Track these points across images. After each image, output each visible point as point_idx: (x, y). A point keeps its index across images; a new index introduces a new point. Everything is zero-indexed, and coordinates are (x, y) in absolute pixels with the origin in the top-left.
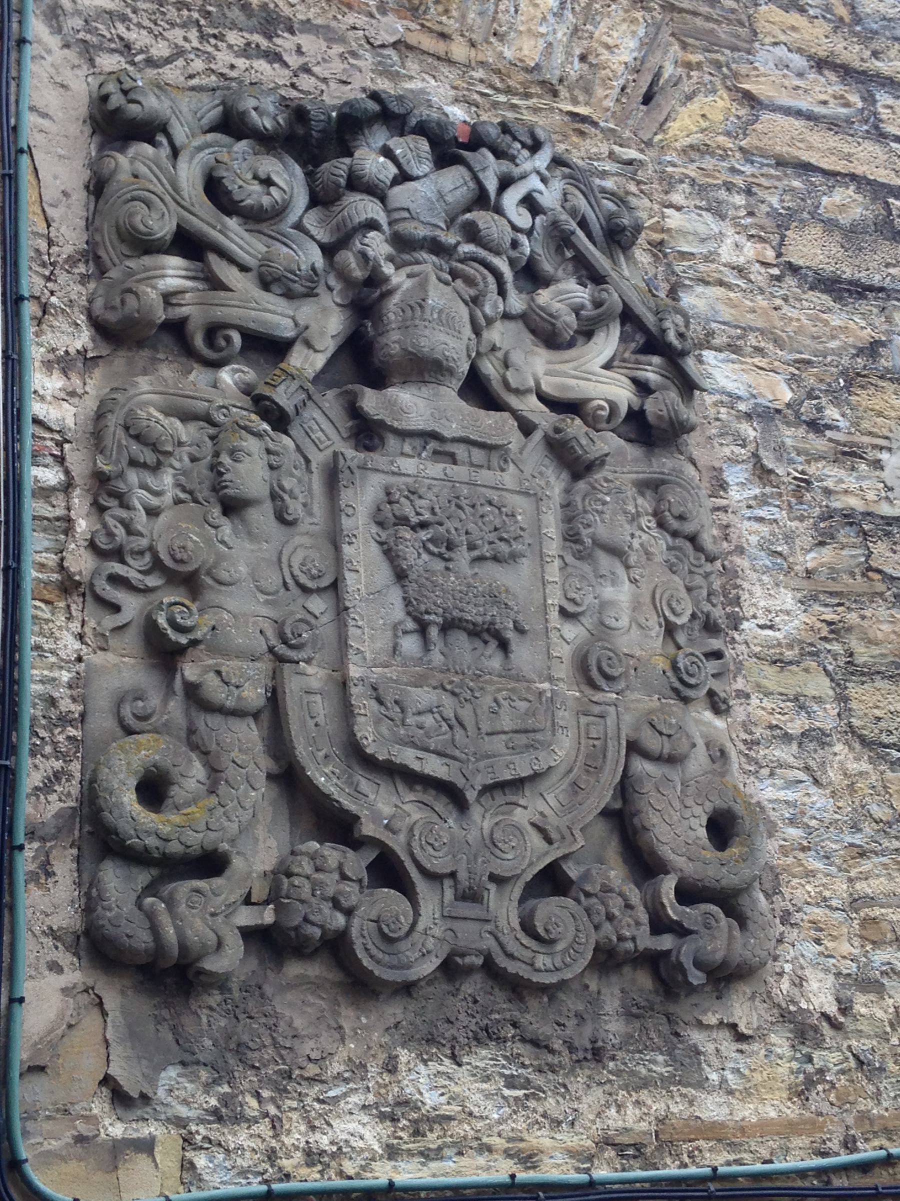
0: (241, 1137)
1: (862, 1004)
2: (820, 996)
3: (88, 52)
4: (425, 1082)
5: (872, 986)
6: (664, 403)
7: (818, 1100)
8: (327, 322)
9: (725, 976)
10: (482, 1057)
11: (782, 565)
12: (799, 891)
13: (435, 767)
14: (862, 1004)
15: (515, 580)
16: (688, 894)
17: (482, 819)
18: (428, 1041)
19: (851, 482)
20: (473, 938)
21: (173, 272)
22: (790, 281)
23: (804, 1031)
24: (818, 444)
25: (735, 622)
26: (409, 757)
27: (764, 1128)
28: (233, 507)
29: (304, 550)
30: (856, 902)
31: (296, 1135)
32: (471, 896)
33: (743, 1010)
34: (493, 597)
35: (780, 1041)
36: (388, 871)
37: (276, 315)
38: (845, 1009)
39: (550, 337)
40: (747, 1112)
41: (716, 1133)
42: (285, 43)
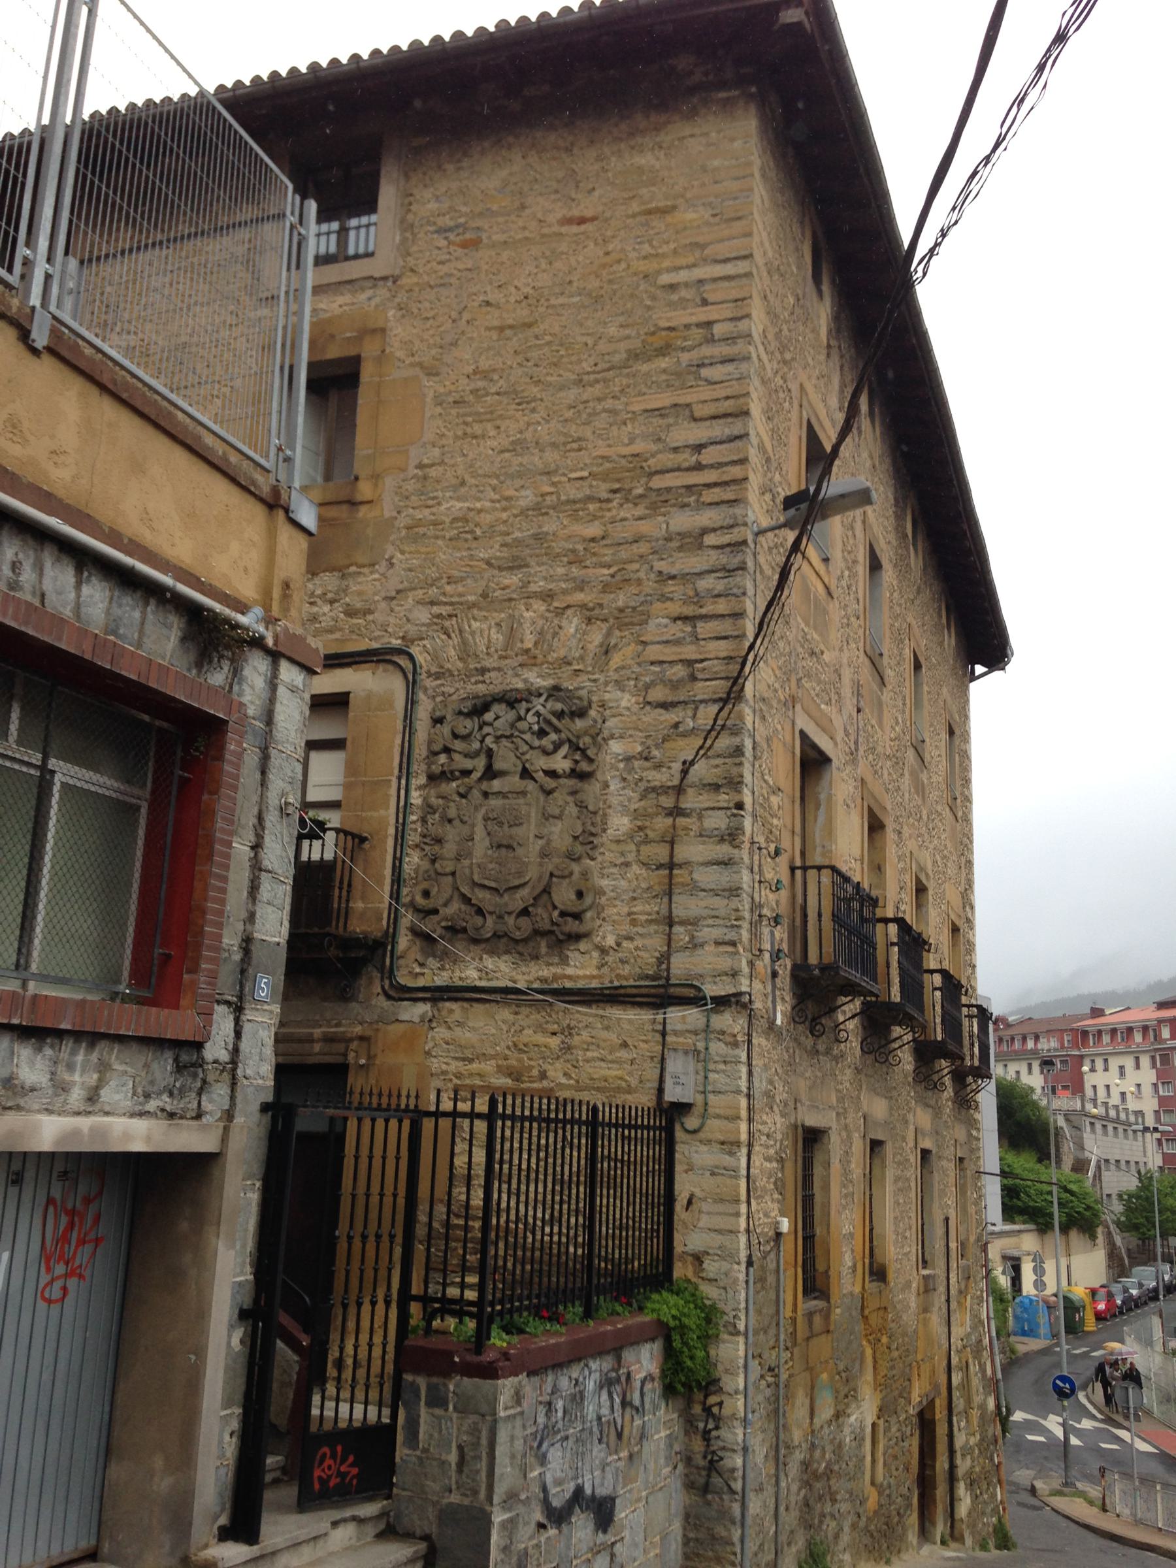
0: (444, 974)
1: (625, 944)
2: (610, 941)
3: (434, 698)
4: (489, 962)
5: (630, 938)
6: (584, 766)
7: (605, 970)
8: (480, 763)
9: (578, 937)
10: (506, 957)
11: (625, 811)
12: (610, 911)
13: (493, 885)
14: (625, 944)
15: (519, 831)
16: (563, 914)
17: (506, 897)
18: (492, 953)
19: (658, 776)
20: (501, 928)
21: (443, 758)
22: (648, 708)
23: (603, 951)
24: (647, 764)
25: (604, 830)
26: (486, 882)
27: (585, 977)
28: (450, 821)
29: (465, 830)
30: (629, 914)
31: (457, 974)
32: (500, 917)
33: (583, 945)
34: (511, 837)
35: (595, 954)
36: (480, 912)
37: (468, 764)
38: (618, 944)
39: (546, 753)
40: (581, 973)
41: (570, 977)
42: (487, 675)
